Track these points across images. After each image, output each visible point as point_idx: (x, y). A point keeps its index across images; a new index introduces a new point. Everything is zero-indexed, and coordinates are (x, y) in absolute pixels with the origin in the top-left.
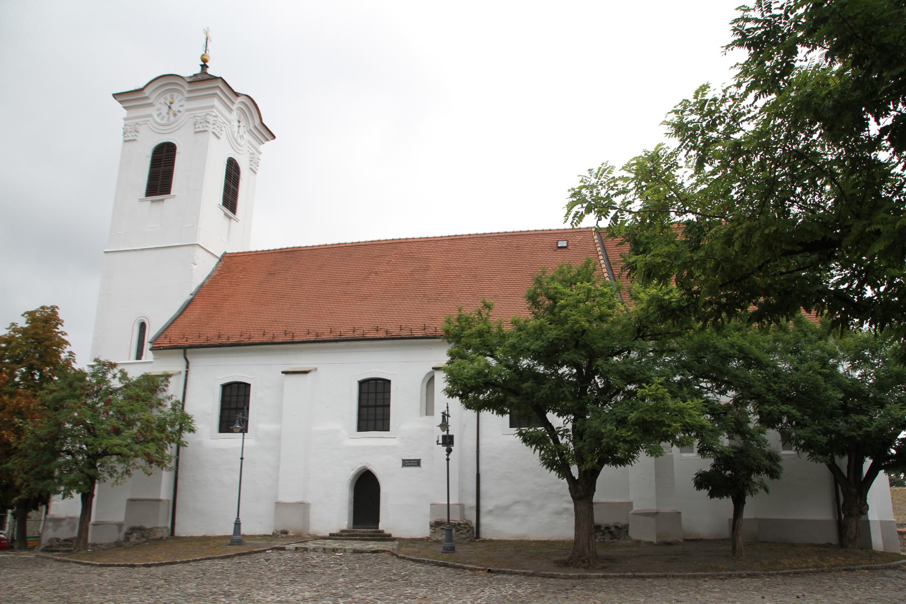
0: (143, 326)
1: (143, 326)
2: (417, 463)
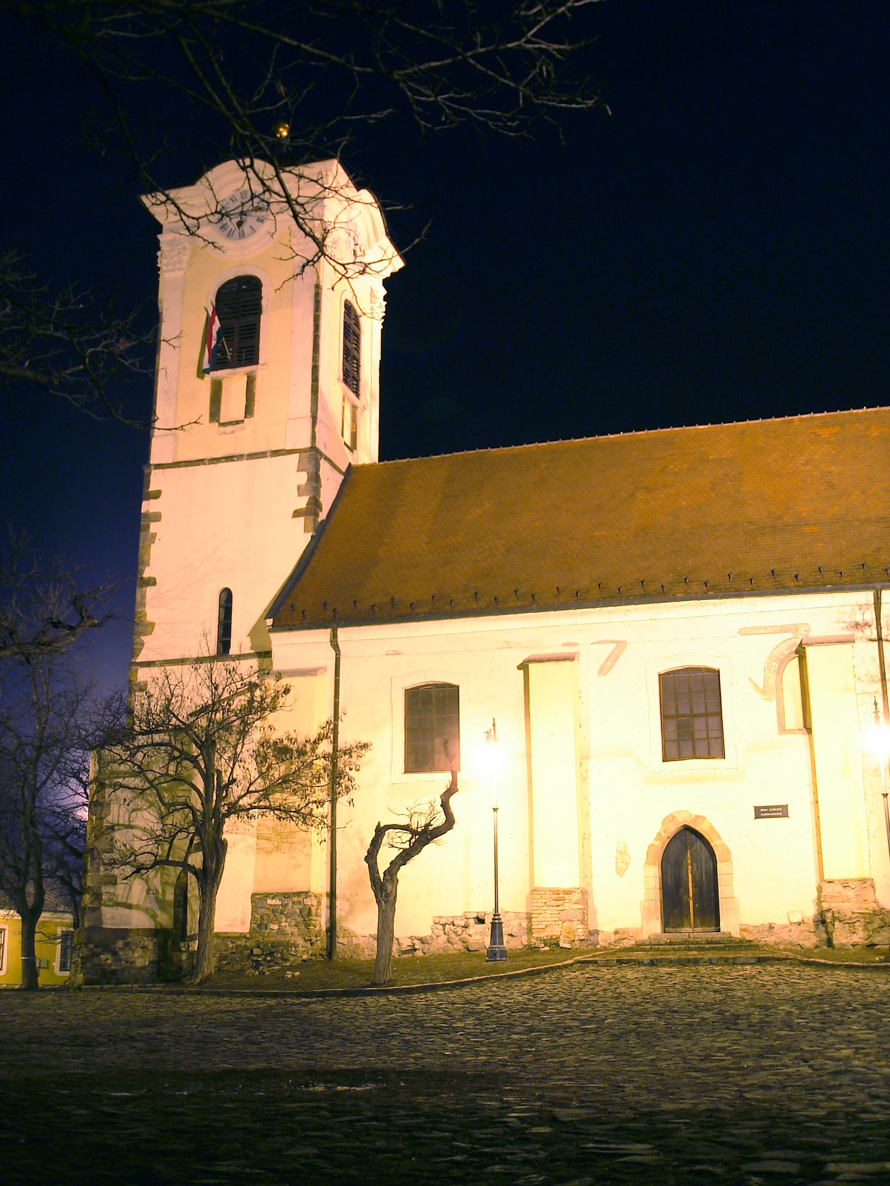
0: (226, 600)
1: (226, 600)
2: (760, 813)
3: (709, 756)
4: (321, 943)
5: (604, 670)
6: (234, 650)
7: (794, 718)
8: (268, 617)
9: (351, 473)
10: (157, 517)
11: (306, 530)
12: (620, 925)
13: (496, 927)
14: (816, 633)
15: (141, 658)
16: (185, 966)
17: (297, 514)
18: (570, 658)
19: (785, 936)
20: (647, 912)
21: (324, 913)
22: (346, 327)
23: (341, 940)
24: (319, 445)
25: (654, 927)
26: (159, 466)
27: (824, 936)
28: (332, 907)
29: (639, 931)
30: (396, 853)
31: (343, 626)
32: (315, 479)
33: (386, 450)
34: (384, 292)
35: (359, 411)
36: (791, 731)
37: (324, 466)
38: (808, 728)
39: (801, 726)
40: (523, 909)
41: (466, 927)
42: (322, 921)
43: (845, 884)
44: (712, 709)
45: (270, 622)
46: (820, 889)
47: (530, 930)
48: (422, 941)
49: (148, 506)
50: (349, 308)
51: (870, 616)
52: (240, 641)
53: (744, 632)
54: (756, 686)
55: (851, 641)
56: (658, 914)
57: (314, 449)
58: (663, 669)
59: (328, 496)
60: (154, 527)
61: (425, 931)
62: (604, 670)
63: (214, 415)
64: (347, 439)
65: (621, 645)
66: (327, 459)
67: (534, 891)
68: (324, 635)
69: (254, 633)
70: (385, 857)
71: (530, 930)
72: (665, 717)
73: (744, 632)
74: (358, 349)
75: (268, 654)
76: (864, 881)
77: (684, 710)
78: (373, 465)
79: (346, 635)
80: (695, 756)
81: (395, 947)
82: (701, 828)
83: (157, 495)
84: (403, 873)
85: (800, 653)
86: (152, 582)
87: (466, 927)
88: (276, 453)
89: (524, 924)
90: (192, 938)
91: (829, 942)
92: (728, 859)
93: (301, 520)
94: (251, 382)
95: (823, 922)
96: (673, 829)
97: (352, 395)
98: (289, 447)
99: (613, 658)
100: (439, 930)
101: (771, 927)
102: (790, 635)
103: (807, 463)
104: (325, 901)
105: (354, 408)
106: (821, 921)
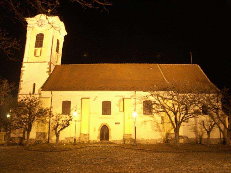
0: (34, 85)
1: (34, 85)
2: (116, 123)
3: (109, 114)
4: (47, 141)
5: (94, 100)
6: (35, 93)
7: (122, 110)
8: (41, 88)
9: (56, 66)
10: (24, 71)
11: (48, 75)
12: (94, 140)
13: (75, 140)
14: (126, 97)
15: (20, 93)
16: (24, 144)
17: (47, 72)
18: (89, 98)
19: (118, 142)
20: (98, 138)
21: (48, 136)
22: (57, 43)
23: (50, 140)
24: (51, 61)
25: (99, 140)
26: (25, 62)
27: (124, 142)
28: (49, 135)
29: (96, 141)
30: (59, 129)
31: (59, 17)
32: (50, 67)
33: (62, 63)
34: (64, 38)
35: (58, 57)
36: (121, 111)
37: (52, 65)
38: (124, 111)
39: (123, 111)
40: (79, 137)
41: (70, 139)
42: (47, 137)
43: (128, 134)
44: (110, 107)
45: (41, 89)
46: (124, 135)
47: (80, 140)
48: (63, 141)
49: (22, 69)
50: (58, 40)
51: (134, 95)
52: (36, 92)
53: (115, 96)
54: (117, 105)
55: (130, 99)
56: (100, 138)
57: (50, 62)
58: (103, 101)
59: (52, 70)
60: (23, 72)
61: (64, 139)
62: (94, 100)
63: (35, 55)
64: (56, 61)
65: (96, 97)
66: (53, 64)
67: (81, 134)
68: (50, 92)
69: (39, 90)
70: (58, 130)
71: (80, 140)
72: (103, 108)
73: (115, 96)
74: (59, 46)
75: (40, 94)
76: (130, 134)
77: (106, 107)
78: (60, 65)
79: (54, 92)
80: (107, 114)
81: (59, 142)
82: (107, 125)
83: (24, 67)
84: (61, 132)
85: (123, 100)
86: (22, 81)
87: (70, 139)
88: (44, 62)
89: (79, 139)
90: (26, 139)
91: (125, 143)
92: (110, 130)
93: (48, 73)
94: (41, 50)
95: (124, 140)
96: (103, 125)
97: (57, 54)
98: (46, 61)
99: (95, 99)
100: (66, 139)
101: (116, 141)
102: (122, 97)
103: (126, 71)
104: (48, 134)
105: (57, 56)
106: (124, 140)
